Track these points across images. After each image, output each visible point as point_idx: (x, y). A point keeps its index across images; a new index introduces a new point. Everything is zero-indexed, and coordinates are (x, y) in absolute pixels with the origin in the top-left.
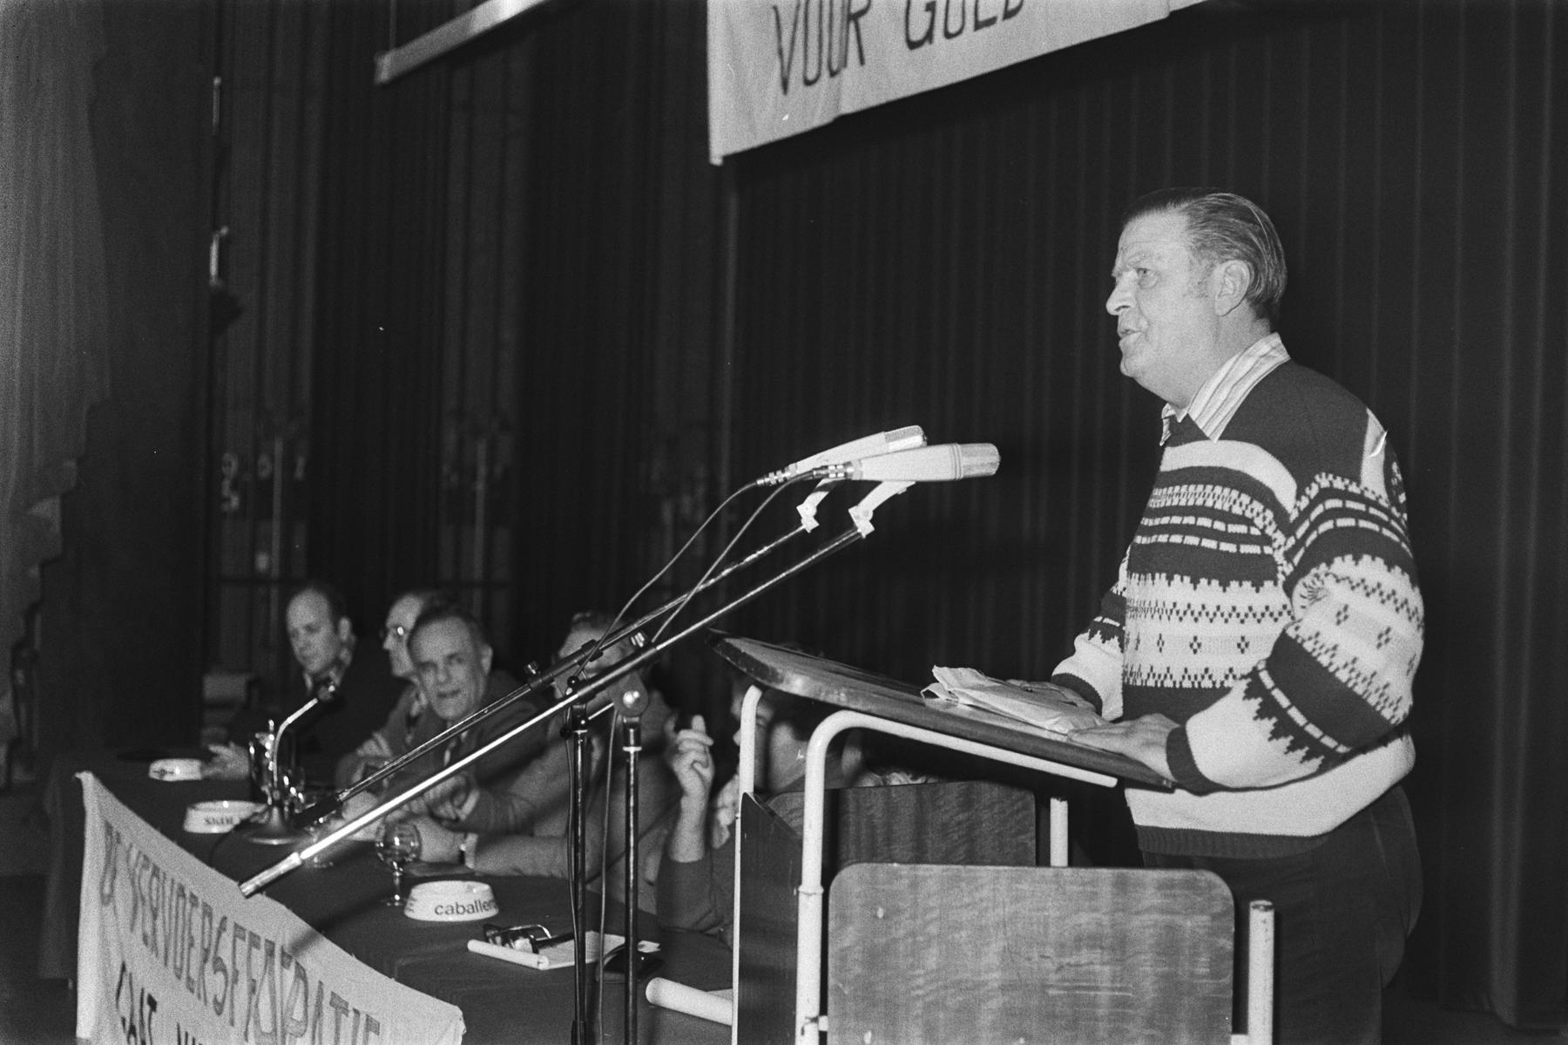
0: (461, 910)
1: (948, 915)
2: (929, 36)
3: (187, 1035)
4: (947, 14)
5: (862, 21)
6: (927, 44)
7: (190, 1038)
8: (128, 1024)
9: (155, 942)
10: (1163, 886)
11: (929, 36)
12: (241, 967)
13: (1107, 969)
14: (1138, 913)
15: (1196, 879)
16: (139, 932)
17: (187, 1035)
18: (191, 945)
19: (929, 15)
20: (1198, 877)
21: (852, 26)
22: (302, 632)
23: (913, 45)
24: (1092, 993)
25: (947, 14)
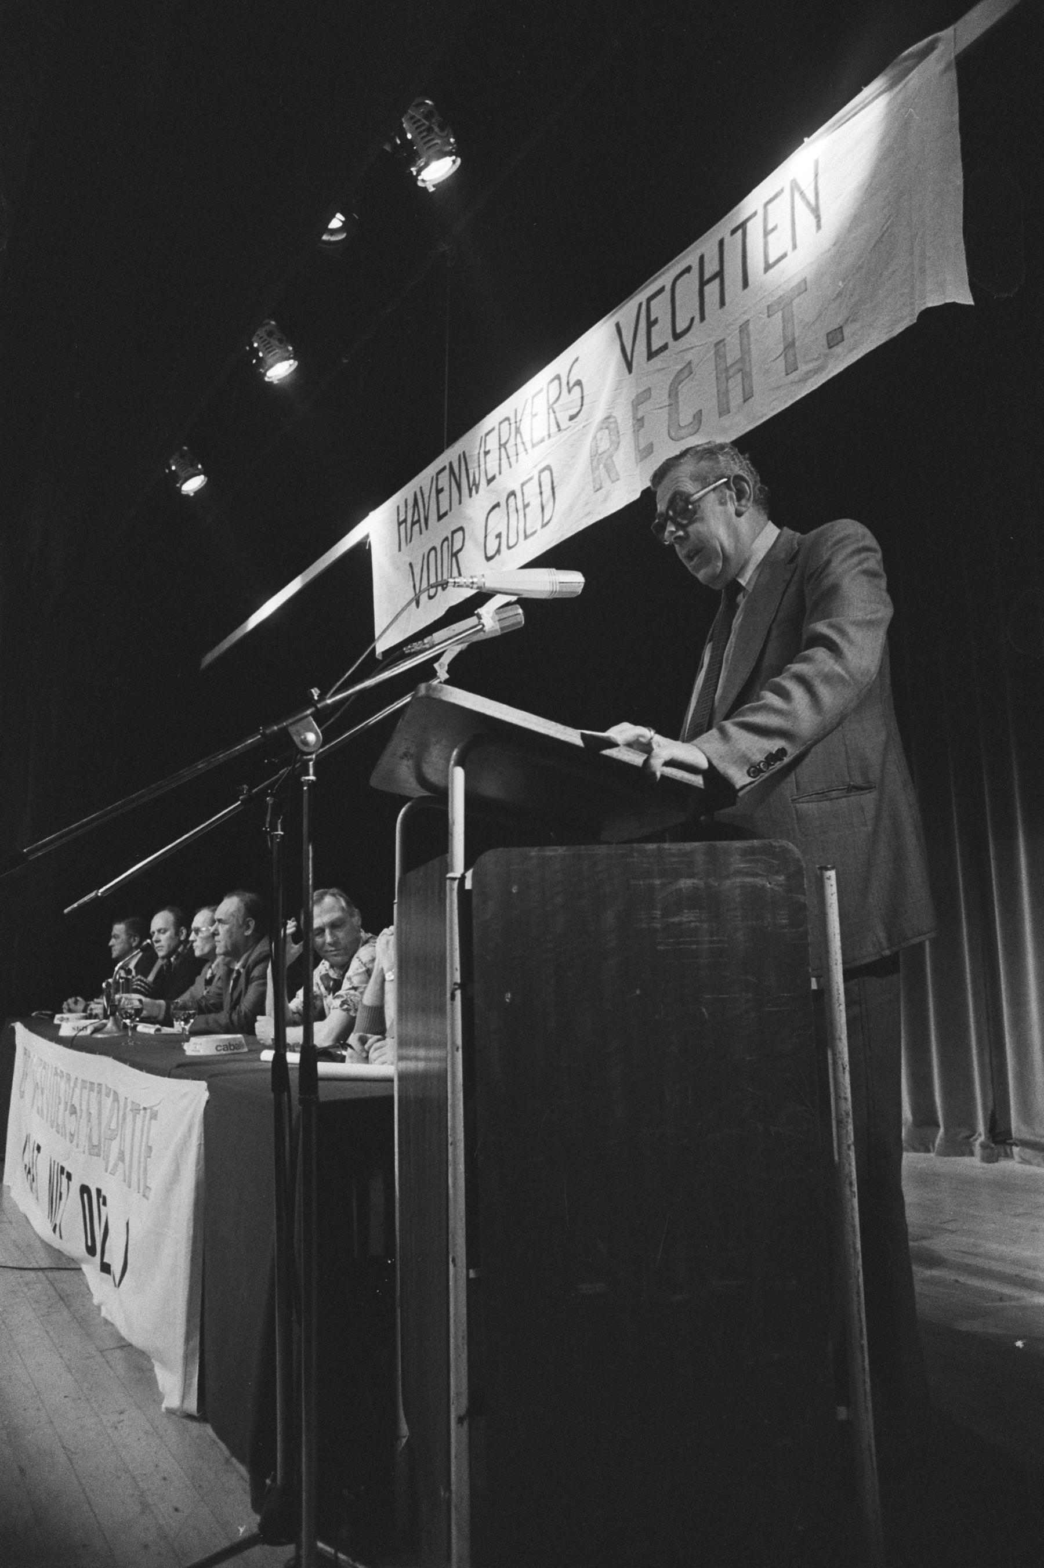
0: (232, 1048)
1: (731, 470)
2: (498, 551)
3: (54, 1161)
4: (508, 537)
5: (460, 555)
6: (497, 555)
7: (56, 1164)
8: (27, 1169)
9: (43, 1113)
10: (745, 853)
11: (498, 551)
12: (84, 1108)
13: (705, 926)
14: (727, 877)
15: (771, 845)
16: (36, 1108)
17: (54, 1161)
18: (60, 1103)
19: (498, 539)
20: (774, 844)
21: (454, 559)
22: (156, 933)
23: (489, 559)
24: (694, 946)
25: (508, 537)
